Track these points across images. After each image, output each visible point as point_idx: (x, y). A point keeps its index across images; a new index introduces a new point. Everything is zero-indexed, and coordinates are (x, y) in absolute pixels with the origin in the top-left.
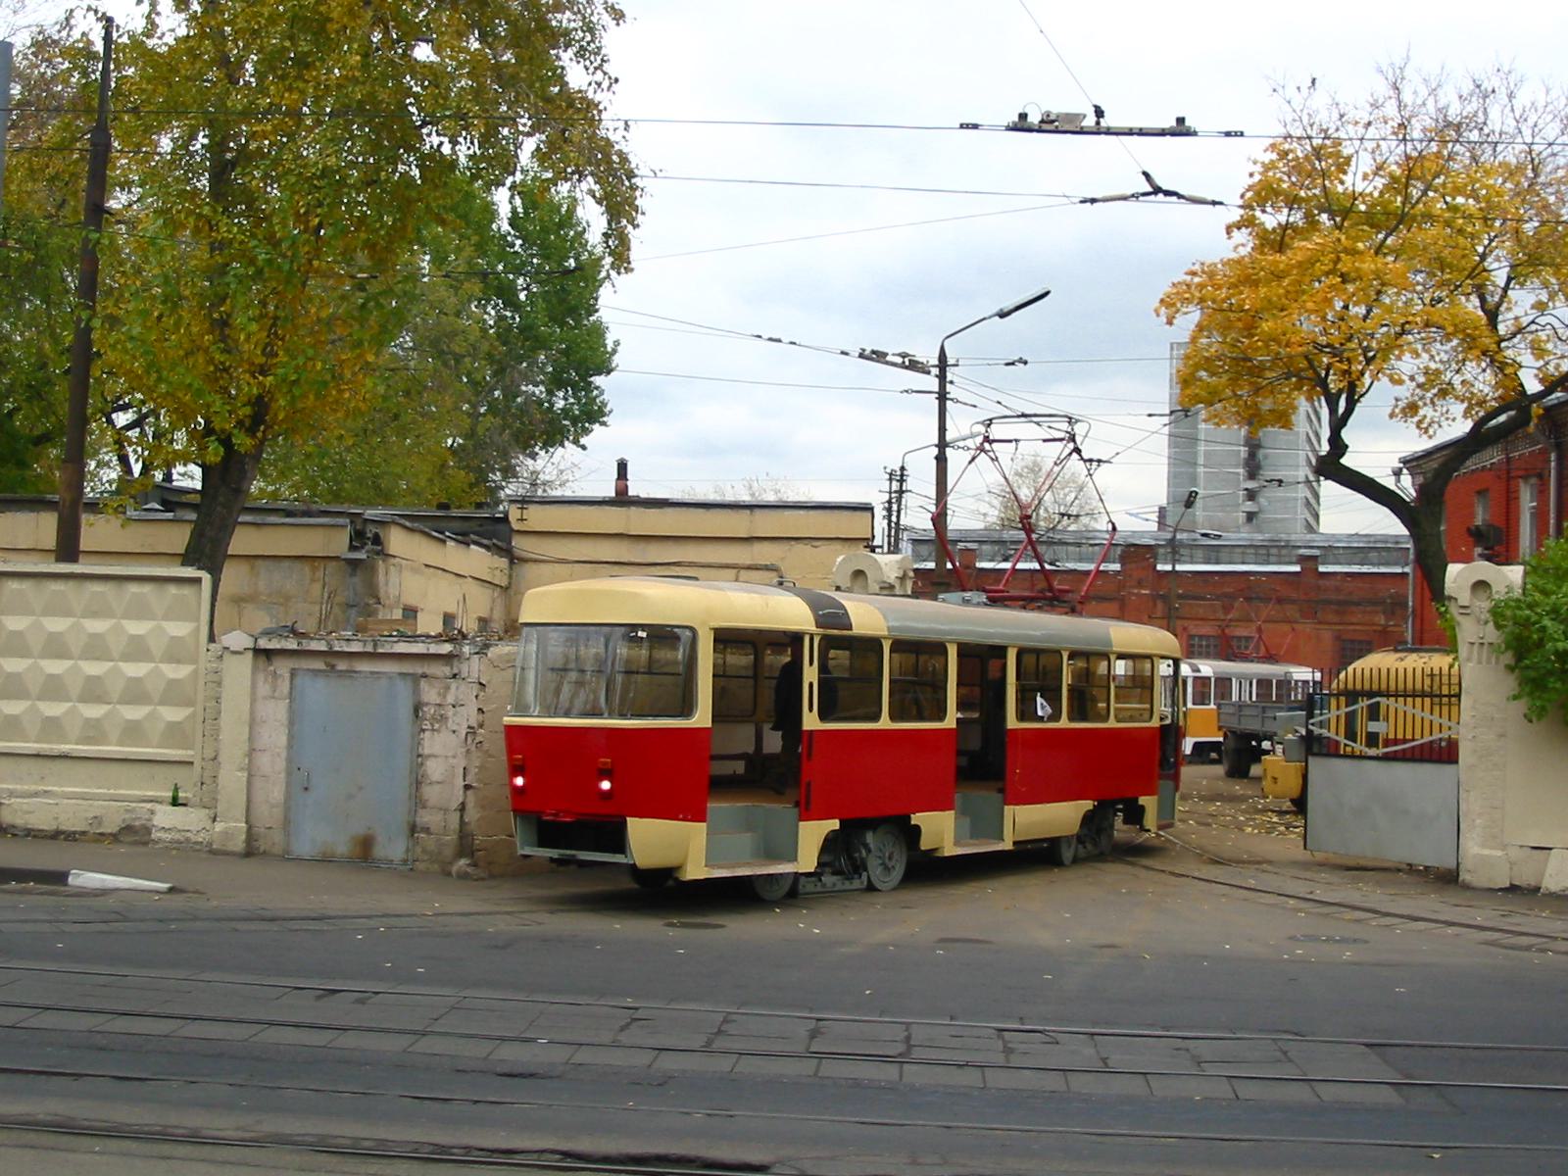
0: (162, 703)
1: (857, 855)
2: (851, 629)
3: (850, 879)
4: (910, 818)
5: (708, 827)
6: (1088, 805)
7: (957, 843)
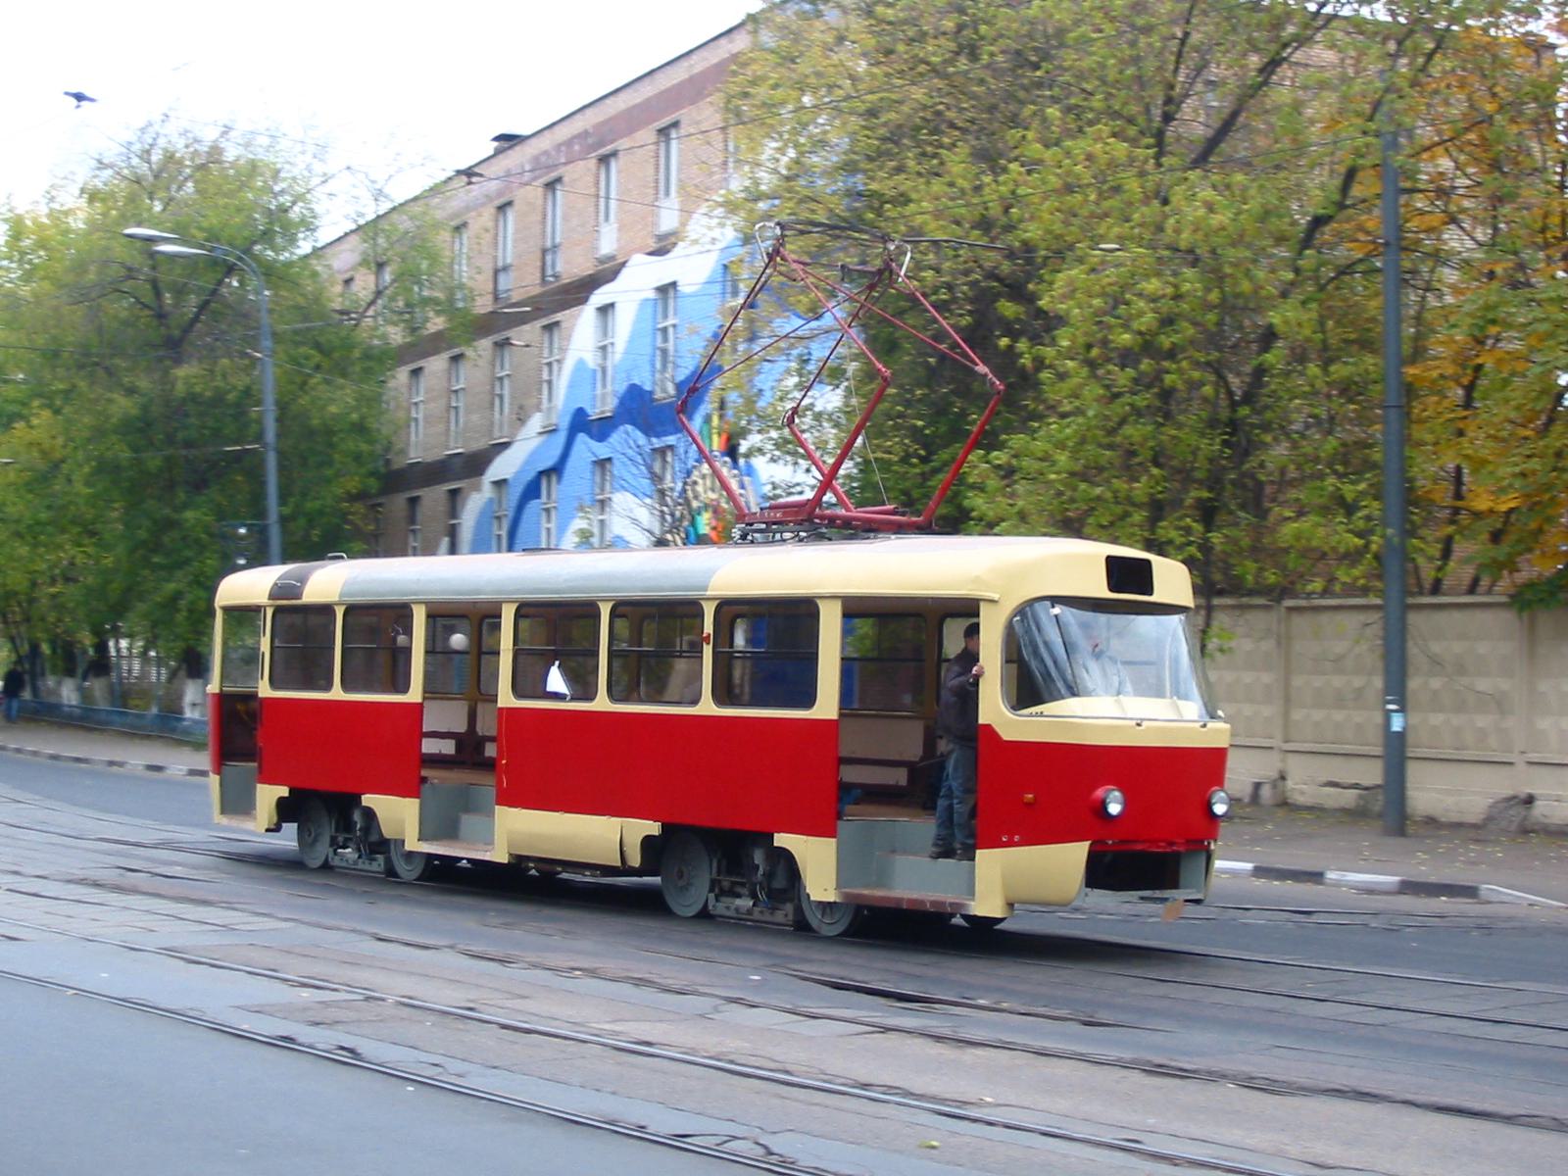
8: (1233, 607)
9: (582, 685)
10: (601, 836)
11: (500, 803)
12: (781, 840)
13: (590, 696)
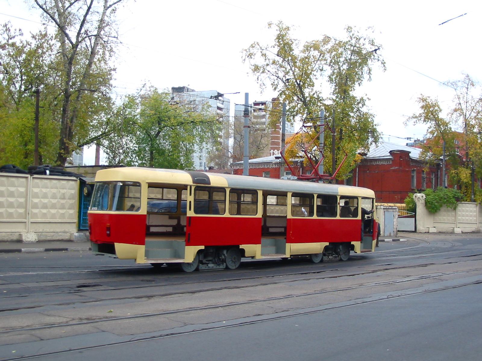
0: (51, 208)
1: (221, 258)
2: (210, 184)
3: (219, 265)
4: (239, 246)
5: (146, 247)
6: (327, 244)
7: (262, 255)
8: (128, 193)
9: (311, 213)
10: (316, 247)
11: (187, 245)
12: (241, 247)
13: (312, 215)
